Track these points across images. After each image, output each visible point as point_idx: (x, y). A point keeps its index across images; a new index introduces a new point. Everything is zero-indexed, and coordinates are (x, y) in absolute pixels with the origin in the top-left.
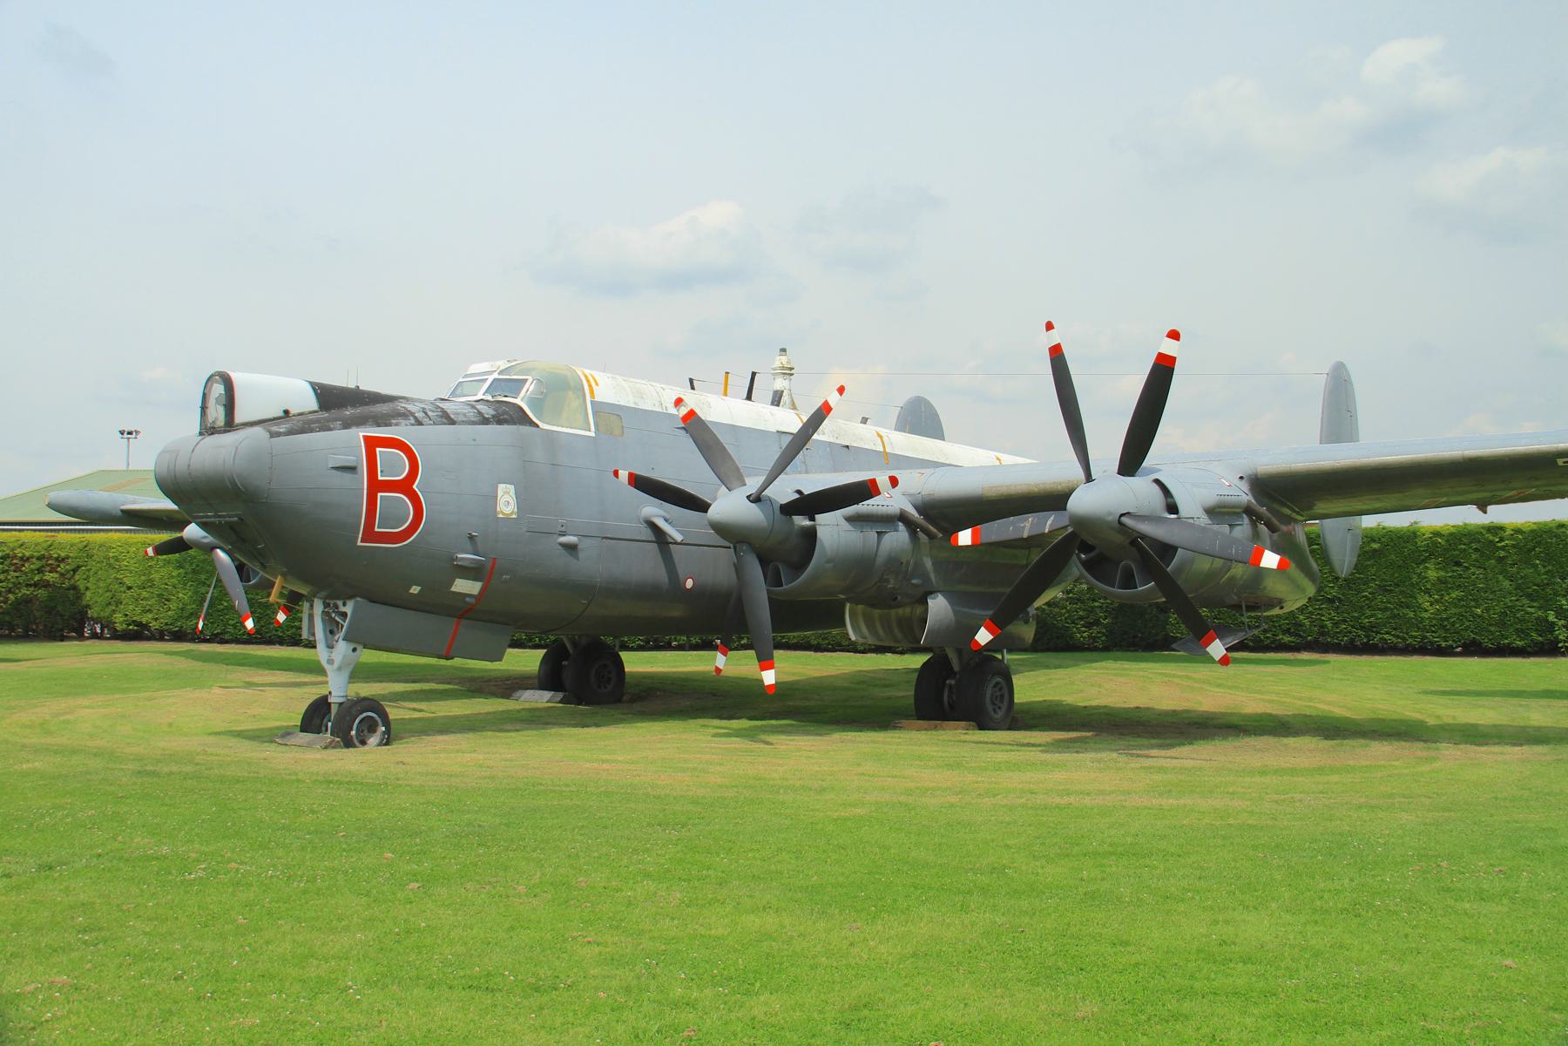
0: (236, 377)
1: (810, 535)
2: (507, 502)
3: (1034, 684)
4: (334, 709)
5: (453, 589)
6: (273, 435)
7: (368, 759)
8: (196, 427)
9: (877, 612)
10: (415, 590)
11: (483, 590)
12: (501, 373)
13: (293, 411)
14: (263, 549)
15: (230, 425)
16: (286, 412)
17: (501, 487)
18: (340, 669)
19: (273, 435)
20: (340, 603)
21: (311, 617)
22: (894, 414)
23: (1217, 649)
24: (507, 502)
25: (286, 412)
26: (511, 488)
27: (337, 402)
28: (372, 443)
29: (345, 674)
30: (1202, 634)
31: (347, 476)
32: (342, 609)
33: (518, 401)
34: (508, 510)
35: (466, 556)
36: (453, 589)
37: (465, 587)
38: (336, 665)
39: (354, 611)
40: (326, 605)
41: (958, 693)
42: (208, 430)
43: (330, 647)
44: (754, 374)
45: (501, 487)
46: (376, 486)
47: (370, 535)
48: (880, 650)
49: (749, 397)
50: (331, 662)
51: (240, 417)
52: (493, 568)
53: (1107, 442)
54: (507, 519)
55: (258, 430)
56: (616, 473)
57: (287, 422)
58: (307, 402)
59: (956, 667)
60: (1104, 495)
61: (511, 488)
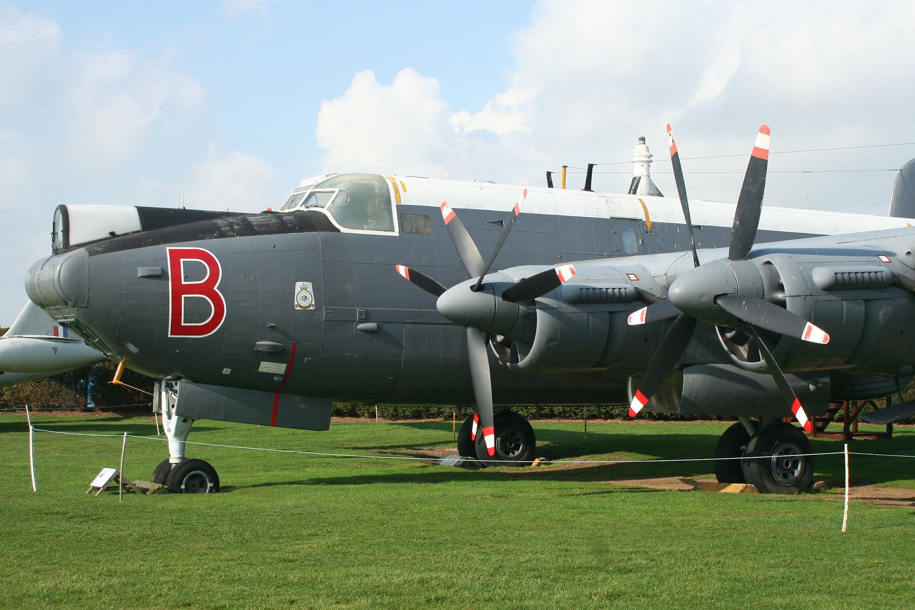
0: (71, 209)
2: (304, 295)
5: (260, 370)
8: (50, 252)
11: (288, 370)
12: (316, 187)
22: (887, 188)
24: (304, 295)
26: (309, 285)
27: (159, 223)
31: (159, 282)
33: (324, 211)
35: (264, 344)
36: (260, 370)
39: (181, 388)
42: (56, 252)
44: (591, 167)
45: (299, 285)
46: (179, 290)
48: (661, 417)
49: (588, 187)
51: (73, 242)
52: (294, 351)
54: (305, 310)
55: (82, 250)
57: (116, 242)
58: (133, 223)
61: (309, 285)
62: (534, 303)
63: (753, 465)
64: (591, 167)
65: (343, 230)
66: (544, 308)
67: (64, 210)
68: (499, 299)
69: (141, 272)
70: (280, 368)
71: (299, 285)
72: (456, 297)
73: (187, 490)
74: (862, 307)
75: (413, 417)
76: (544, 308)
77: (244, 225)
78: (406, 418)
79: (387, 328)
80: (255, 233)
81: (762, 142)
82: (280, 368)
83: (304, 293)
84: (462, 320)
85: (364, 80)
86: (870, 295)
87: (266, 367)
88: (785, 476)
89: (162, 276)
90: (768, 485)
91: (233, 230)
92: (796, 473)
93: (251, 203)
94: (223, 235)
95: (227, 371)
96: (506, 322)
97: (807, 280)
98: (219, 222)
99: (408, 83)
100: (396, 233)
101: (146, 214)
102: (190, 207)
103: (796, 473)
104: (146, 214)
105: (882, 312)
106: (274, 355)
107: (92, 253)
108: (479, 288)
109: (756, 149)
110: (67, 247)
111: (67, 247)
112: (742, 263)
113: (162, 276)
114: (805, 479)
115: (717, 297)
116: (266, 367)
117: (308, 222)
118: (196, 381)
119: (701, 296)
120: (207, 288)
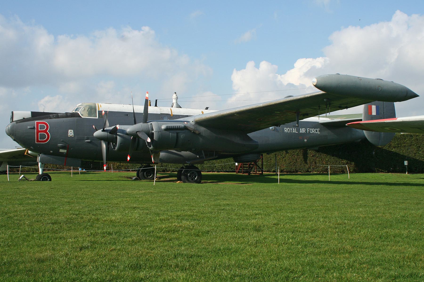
0: (14, 112)
2: (71, 133)
11: (67, 151)
24: (71, 133)
27: (36, 115)
33: (79, 112)
35: (60, 145)
44: (156, 100)
45: (69, 131)
46: (38, 131)
51: (14, 120)
54: (71, 137)
57: (24, 120)
61: (72, 131)
62: (117, 134)
63: (157, 174)
64: (156, 100)
65: (82, 117)
66: (119, 136)
67: (12, 113)
68: (108, 133)
69: (29, 127)
70: (65, 151)
71: (69, 131)
72: (98, 133)
73: (42, 181)
74: (176, 135)
75: (163, 172)
76: (119, 136)
77: (57, 116)
78: (160, 172)
79: (93, 141)
80: (59, 118)
81: (147, 95)
82: (65, 151)
83: (71, 133)
84: (101, 138)
85: (250, 65)
86: (178, 131)
87: (61, 151)
88: (192, 179)
89: (34, 128)
90: (186, 181)
91: (53, 117)
92: (196, 179)
93: (62, 110)
94: (51, 118)
95: (51, 152)
96: (110, 139)
97: (160, 128)
98: (51, 115)
99: (264, 65)
100: (97, 118)
101: (33, 113)
102: (46, 111)
103: (196, 179)
104: (33, 113)
105: (182, 136)
106: (63, 148)
107: (17, 123)
108: (104, 131)
109: (146, 97)
110: (13, 121)
111: (13, 121)
112: (145, 124)
113: (34, 128)
114: (198, 180)
115: (137, 132)
116: (61, 151)
117: (75, 115)
118: (45, 154)
119: (133, 132)
120: (45, 131)
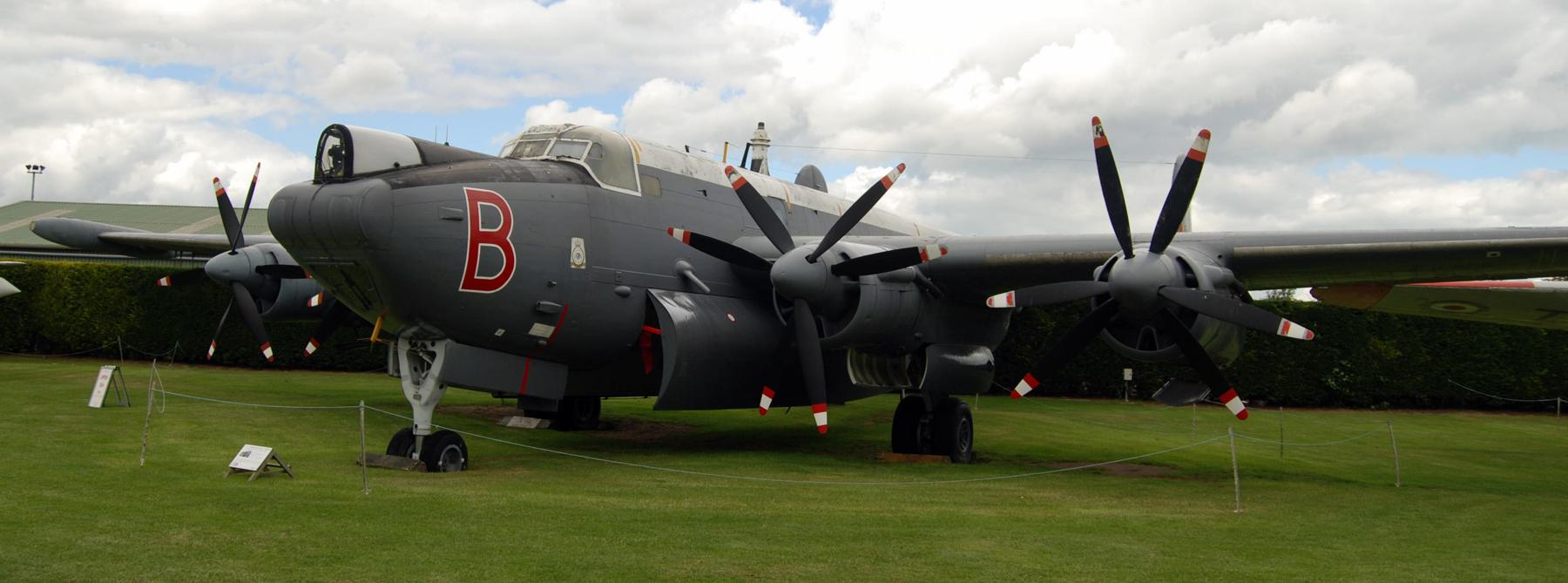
1: (854, 295)
2: (578, 253)
3: (992, 422)
4: (419, 442)
6: (395, 186)
7: (451, 487)
9: (865, 356)
10: (500, 332)
13: (402, 164)
14: (363, 289)
15: (349, 176)
16: (397, 165)
17: (574, 240)
18: (427, 404)
19: (395, 186)
20: (428, 343)
21: (396, 354)
23: (1236, 405)
24: (578, 253)
25: (397, 165)
26: (581, 241)
28: (474, 197)
29: (431, 409)
30: (1218, 398)
32: (431, 349)
34: (578, 262)
37: (541, 330)
38: (424, 400)
40: (413, 345)
41: (931, 432)
43: (417, 383)
45: (574, 240)
47: (471, 282)
50: (417, 397)
51: (358, 168)
53: (1143, 222)
54: (578, 270)
56: (671, 232)
59: (929, 409)
60: (1141, 266)
61: (581, 241)
